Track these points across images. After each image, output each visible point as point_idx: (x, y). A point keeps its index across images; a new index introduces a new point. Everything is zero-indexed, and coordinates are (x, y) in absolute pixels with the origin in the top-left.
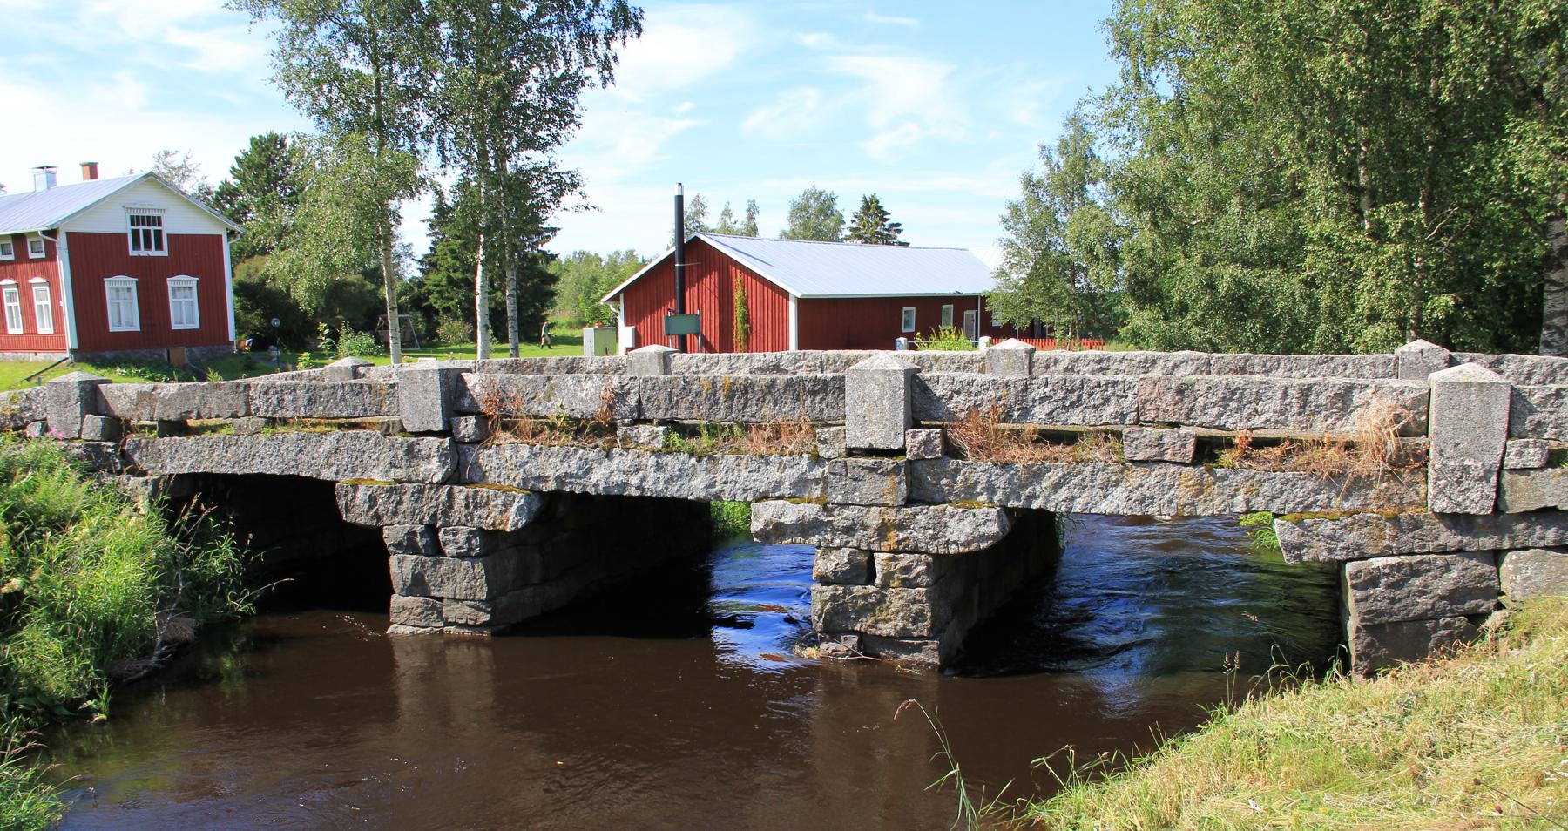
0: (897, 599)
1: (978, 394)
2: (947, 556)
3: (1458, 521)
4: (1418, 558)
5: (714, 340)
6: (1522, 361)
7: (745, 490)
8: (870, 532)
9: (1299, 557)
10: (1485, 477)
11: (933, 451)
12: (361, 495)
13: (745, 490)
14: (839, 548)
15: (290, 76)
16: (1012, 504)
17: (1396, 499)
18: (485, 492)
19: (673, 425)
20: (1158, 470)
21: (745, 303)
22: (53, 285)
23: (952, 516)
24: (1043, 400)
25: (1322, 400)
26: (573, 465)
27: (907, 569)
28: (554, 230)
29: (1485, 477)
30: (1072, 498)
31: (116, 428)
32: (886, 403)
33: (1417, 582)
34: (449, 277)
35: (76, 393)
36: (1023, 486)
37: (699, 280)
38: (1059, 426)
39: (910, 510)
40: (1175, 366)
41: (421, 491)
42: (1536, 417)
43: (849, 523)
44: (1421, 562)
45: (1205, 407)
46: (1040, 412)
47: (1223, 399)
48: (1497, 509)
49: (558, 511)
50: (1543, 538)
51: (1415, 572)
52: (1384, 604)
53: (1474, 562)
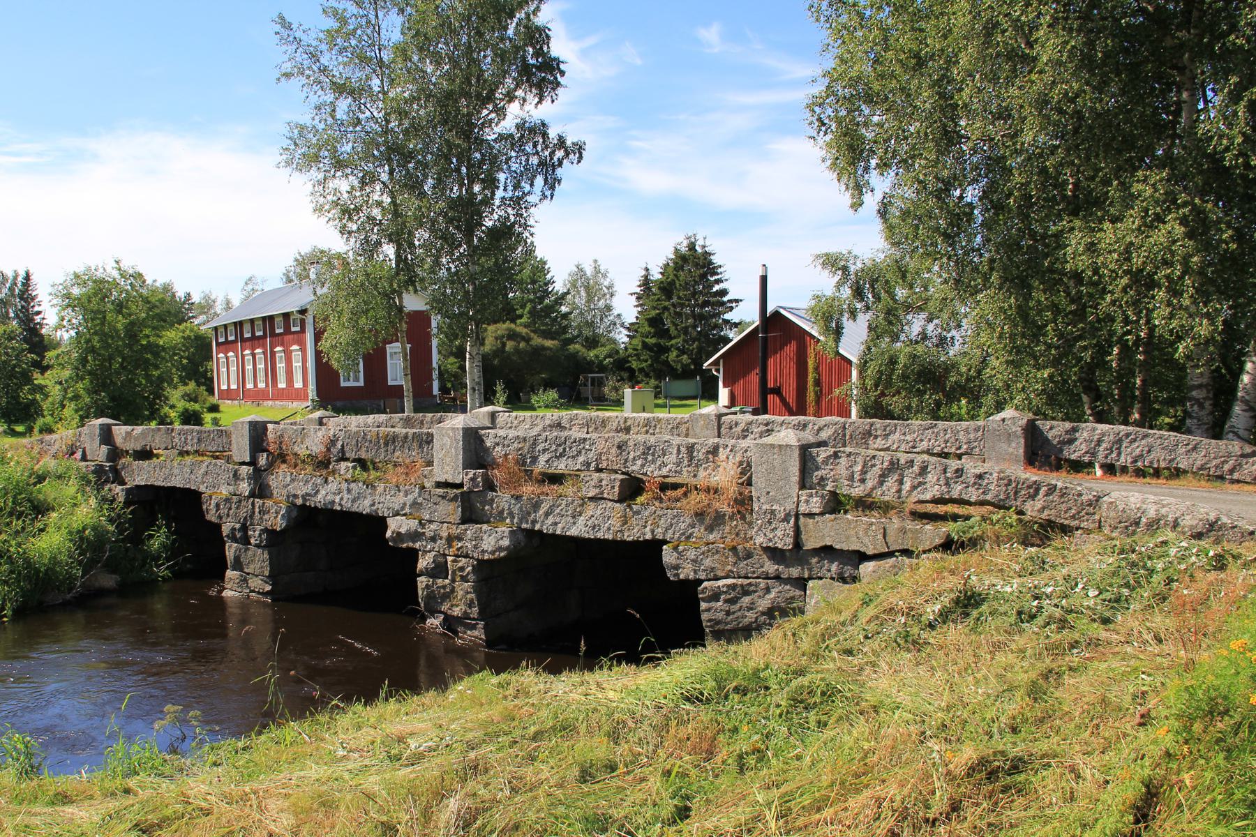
2: (483, 560)
3: (774, 553)
4: (747, 581)
5: (792, 401)
9: (677, 575)
10: (786, 519)
11: (477, 486)
12: (213, 502)
15: (319, 209)
16: (524, 526)
17: (742, 535)
18: (269, 503)
19: (362, 463)
20: (603, 505)
21: (816, 369)
22: (303, 350)
24: (545, 450)
25: (701, 456)
26: (309, 488)
27: (462, 569)
28: (737, 301)
29: (786, 519)
30: (556, 524)
31: (115, 454)
33: (746, 600)
34: (644, 342)
35: (98, 431)
37: (781, 349)
38: (552, 471)
39: (463, 527)
40: (820, 429)
41: (240, 501)
42: (819, 473)
44: (750, 584)
45: (634, 459)
47: (644, 453)
48: (798, 544)
49: (309, 519)
50: (829, 571)
51: (746, 593)
52: (721, 615)
53: (788, 587)
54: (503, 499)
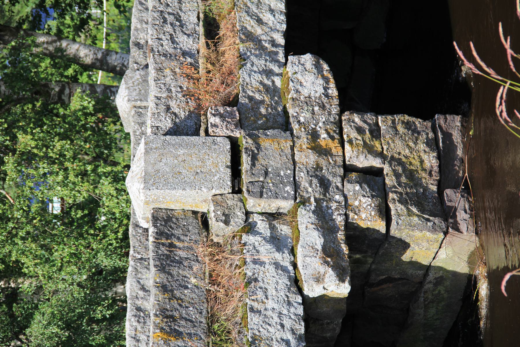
0: (398, 147)
1: (170, 91)
6: (137, 29)
7: (289, 303)
8: (323, 162)
13: (289, 303)
14: (345, 197)
23: (297, 91)
30: (272, 11)
32: (181, 152)
36: (263, 48)
38: (201, 30)
39: (295, 126)
43: (315, 181)
46: (186, 43)
54: (250, 81)
